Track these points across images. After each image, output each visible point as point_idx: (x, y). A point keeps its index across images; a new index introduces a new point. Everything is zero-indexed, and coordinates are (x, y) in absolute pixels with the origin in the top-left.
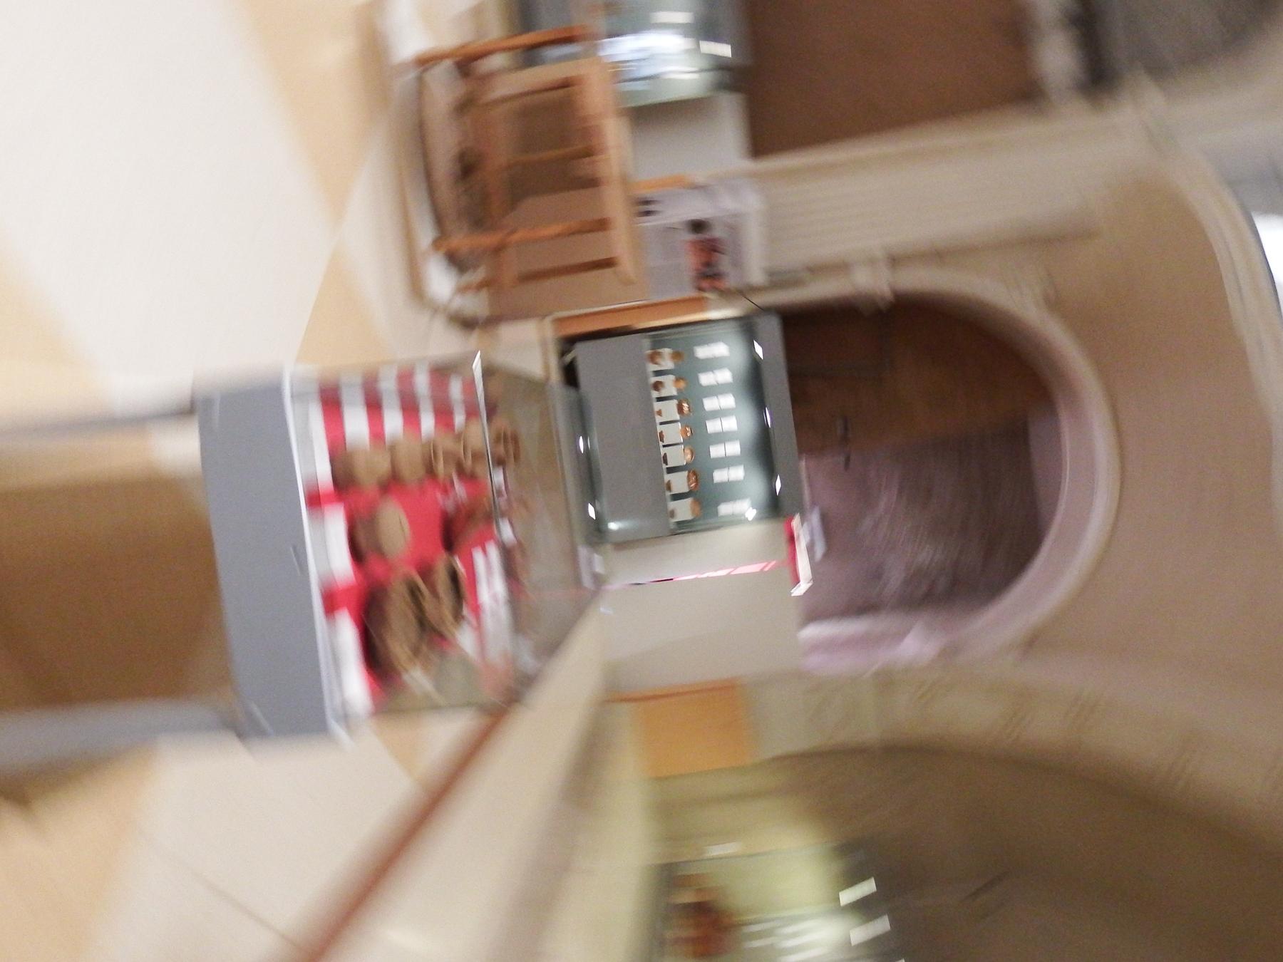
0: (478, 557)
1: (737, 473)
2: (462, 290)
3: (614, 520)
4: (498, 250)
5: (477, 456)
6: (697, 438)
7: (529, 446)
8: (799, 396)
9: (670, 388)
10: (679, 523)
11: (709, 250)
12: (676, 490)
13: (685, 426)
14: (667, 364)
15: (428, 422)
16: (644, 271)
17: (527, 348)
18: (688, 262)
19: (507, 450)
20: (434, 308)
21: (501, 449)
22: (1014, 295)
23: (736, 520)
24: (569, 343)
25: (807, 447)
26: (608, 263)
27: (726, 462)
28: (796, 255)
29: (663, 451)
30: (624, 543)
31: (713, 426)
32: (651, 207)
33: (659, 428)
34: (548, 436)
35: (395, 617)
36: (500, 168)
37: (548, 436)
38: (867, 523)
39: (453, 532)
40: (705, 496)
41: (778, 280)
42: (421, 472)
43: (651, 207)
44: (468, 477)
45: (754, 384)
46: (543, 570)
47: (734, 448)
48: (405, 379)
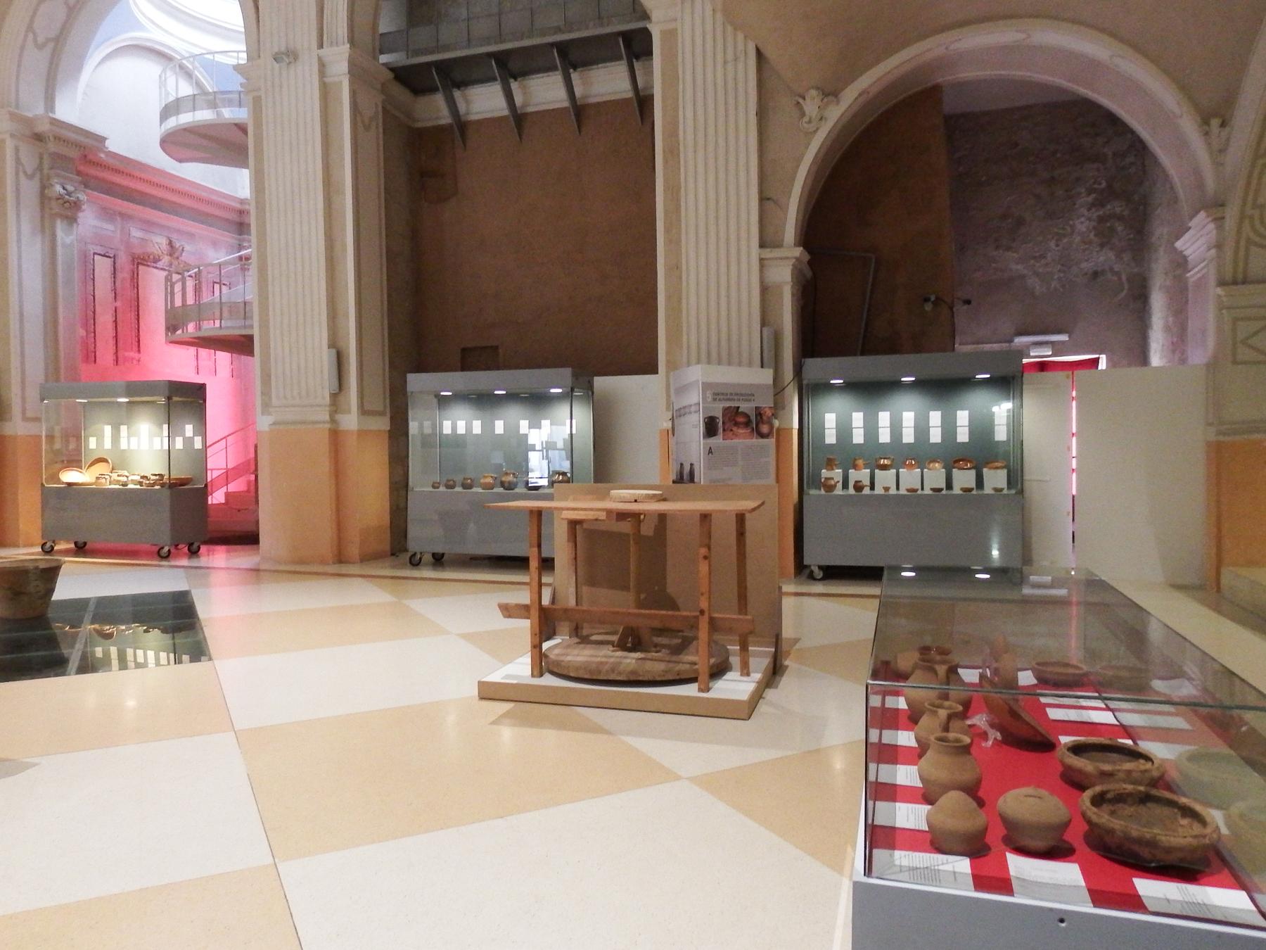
1: (963, 417)
2: (745, 671)
4: (714, 625)
6: (919, 454)
8: (891, 347)
9: (862, 475)
10: (1009, 488)
11: (734, 420)
12: (973, 485)
13: (904, 465)
14: (837, 474)
15: (906, 738)
17: (830, 620)
18: (743, 442)
20: (757, 696)
23: (1015, 423)
24: (801, 569)
25: (947, 344)
27: (949, 428)
29: (927, 491)
31: (908, 437)
32: (687, 469)
33: (903, 491)
38: (1034, 283)
39: (1028, 739)
40: (980, 453)
41: (770, 357)
43: (687, 469)
44: (967, 707)
45: (871, 390)
46: (1070, 642)
47: (935, 418)
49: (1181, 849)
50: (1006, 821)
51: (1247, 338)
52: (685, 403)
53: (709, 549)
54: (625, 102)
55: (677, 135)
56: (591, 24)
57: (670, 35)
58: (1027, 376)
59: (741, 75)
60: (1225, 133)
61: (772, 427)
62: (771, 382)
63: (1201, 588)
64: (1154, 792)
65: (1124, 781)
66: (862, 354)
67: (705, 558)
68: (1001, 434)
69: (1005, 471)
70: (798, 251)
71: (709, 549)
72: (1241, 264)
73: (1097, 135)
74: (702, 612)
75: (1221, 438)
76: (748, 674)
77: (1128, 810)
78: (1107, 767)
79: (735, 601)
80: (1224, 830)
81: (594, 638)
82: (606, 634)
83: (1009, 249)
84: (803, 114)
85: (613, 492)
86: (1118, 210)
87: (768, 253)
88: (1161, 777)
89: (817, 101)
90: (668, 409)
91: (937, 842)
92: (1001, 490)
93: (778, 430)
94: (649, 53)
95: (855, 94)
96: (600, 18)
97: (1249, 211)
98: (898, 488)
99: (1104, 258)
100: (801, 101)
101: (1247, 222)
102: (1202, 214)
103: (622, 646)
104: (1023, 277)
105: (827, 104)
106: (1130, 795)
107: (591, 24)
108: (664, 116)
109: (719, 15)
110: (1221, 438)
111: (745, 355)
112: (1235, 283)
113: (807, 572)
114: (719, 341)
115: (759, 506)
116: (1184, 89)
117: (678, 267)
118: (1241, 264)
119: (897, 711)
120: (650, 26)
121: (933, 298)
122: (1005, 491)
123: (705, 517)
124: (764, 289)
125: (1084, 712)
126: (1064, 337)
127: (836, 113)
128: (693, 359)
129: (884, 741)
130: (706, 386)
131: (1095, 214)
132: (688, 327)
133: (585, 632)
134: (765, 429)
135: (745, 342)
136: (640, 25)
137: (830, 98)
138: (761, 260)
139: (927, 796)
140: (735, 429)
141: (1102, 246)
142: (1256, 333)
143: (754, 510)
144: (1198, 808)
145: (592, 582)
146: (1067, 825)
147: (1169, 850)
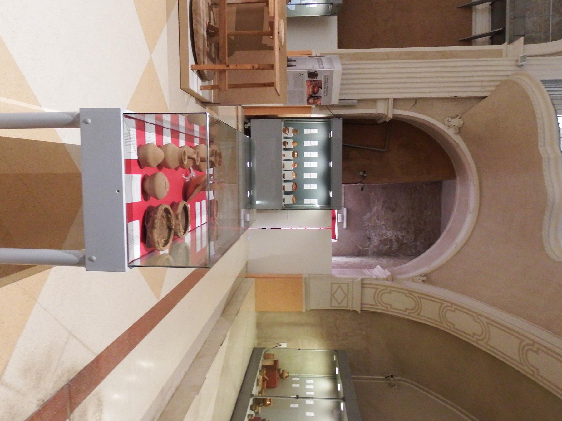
0: (198, 204)
1: (314, 187)
2: (203, 88)
3: (258, 200)
4: (222, 72)
5: (203, 160)
6: (299, 169)
7: (226, 161)
8: (345, 157)
10: (285, 204)
11: (316, 85)
12: (286, 190)
13: (294, 163)
14: (291, 134)
15: (182, 142)
16: (287, 92)
17: (231, 116)
18: (306, 90)
19: (216, 160)
20: (192, 93)
21: (213, 159)
22: (444, 125)
23: (310, 207)
24: (248, 119)
26: (272, 85)
27: (310, 181)
28: (353, 94)
29: (283, 172)
30: (261, 210)
32: (293, 63)
33: (283, 162)
34: (234, 158)
35: (157, 223)
36: (227, 38)
37: (234, 158)
38: (368, 215)
39: (187, 191)
40: (299, 195)
42: (177, 164)
43: (293, 63)
44: (197, 168)
45: (327, 149)
46: (225, 214)
47: (314, 176)
48: (175, 123)
49: (153, 236)
50: (153, 176)
51: (341, 288)
52: (324, 63)
53: (258, 69)
54: (470, 29)
55: (450, 58)
56: (512, 14)
57: (499, 54)
58: (330, 211)
59: (474, 89)
60: (420, 281)
61: (312, 104)
62: (332, 104)
63: (247, 272)
64: (173, 232)
65: (175, 223)
66: (343, 146)
67: (253, 67)
68: (306, 201)
69: (292, 203)
70: (390, 116)
71: (258, 69)
72: (369, 286)
73: (425, 239)
74: (228, 66)
75: (304, 279)
76: (201, 89)
77: (165, 222)
78: (180, 217)
79: (235, 82)
80: (161, 253)
81: (211, 12)
82: (214, 20)
83: (383, 206)
84: (452, 118)
85: (283, 21)
86: (394, 246)
87: (391, 102)
88: (179, 237)
89: (457, 125)
90: (321, 54)
91: (142, 147)
92: (284, 201)
93: (310, 107)
94: (492, 44)
95: (458, 142)
96: (515, 17)
97: (389, 288)
98: (285, 160)
99: (376, 241)
100: (458, 117)
101: (385, 288)
102: (389, 273)
103: (209, 27)
104: (371, 212)
105: (455, 129)
106: (171, 223)
107: (512, 14)
108: (462, 51)
109: (505, 78)
110: (304, 279)
111: (346, 92)
112: (362, 284)
113: (247, 121)
114: (353, 79)
115: (277, 93)
116: (440, 268)
117: (388, 58)
118: (369, 286)
119: (193, 142)
120: (506, 43)
121: (365, 175)
122: (283, 203)
123: (272, 67)
124: (375, 100)
125: (199, 216)
126: (345, 226)
127: (451, 133)
128: (345, 67)
129: (180, 134)
130: (332, 72)
131: (393, 238)
132: (358, 64)
133: (214, 9)
134: (311, 101)
135: (351, 91)
136: (507, 37)
137: (458, 131)
138: (388, 99)
139: (160, 145)
140: (311, 86)
141: (380, 241)
142: (342, 290)
143: (276, 90)
144: (169, 245)
145: (238, 12)
146: (156, 197)
147: (151, 233)
